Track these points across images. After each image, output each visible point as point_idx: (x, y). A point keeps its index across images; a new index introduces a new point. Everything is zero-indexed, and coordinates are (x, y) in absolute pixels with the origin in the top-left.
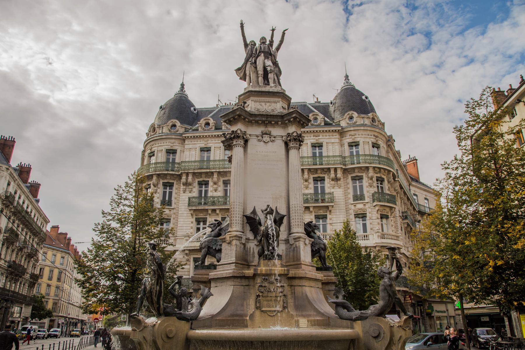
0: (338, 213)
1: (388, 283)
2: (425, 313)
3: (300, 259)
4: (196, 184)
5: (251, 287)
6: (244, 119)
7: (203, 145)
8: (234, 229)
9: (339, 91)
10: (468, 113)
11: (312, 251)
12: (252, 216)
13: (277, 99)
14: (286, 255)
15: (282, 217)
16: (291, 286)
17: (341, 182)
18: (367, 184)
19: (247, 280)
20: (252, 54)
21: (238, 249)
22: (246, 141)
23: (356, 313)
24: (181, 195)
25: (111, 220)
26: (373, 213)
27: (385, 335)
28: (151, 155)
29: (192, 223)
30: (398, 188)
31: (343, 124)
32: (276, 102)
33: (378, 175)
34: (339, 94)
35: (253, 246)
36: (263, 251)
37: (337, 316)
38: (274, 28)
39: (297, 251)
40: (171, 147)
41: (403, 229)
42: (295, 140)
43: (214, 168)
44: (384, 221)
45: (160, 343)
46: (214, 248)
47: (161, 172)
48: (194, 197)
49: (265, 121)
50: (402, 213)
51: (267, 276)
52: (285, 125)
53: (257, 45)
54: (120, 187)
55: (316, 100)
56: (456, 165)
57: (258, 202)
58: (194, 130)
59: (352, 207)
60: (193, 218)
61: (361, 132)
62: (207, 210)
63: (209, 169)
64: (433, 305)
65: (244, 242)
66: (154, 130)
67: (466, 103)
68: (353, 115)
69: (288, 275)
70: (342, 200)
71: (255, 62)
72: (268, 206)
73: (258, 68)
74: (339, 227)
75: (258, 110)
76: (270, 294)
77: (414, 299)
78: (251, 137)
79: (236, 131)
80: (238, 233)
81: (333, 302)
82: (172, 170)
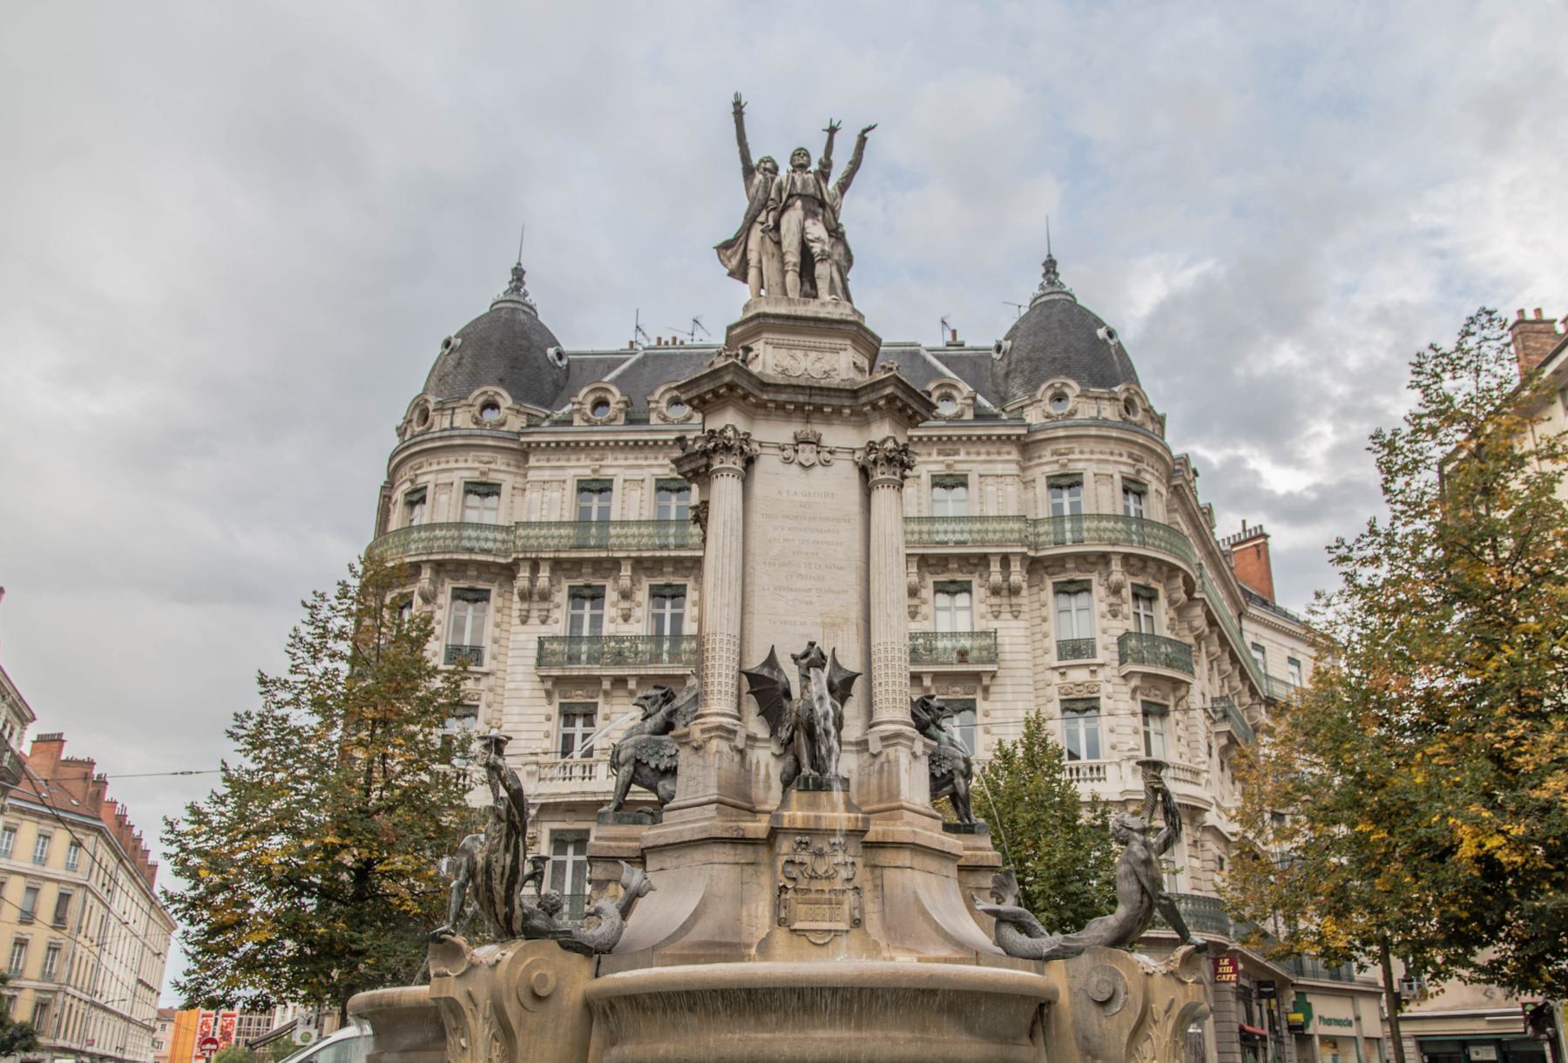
0: (1009, 697)
1: (1142, 855)
2: (1284, 1025)
3: (899, 794)
4: (561, 597)
5: (762, 868)
6: (745, 397)
7: (587, 473)
8: (714, 709)
9: (1024, 311)
10: (1418, 391)
11: (932, 776)
12: (765, 672)
13: (839, 341)
14: (860, 785)
15: (849, 680)
16: (874, 867)
17: (1024, 598)
18: (1104, 608)
19: (750, 849)
20: (767, 199)
21: (725, 765)
22: (750, 461)
23: (1049, 941)
24: (513, 629)
25: (288, 703)
26: (1117, 696)
27: (1130, 997)
28: (416, 497)
29: (549, 719)
30: (1200, 622)
32: (835, 351)
33: (1140, 581)
34: (1023, 319)
35: (767, 761)
36: (798, 769)
37: (1000, 950)
38: (835, 123)
39: (890, 773)
40: (483, 474)
41: (1215, 752)
42: (889, 460)
43: (621, 548)
44: (1154, 725)
45: (512, 1009)
46: (653, 765)
47: (447, 556)
48: (555, 638)
49: (805, 404)
50: (1213, 700)
51: (809, 834)
52: (861, 419)
53: (783, 174)
54: (322, 596)
55: (949, 338)
56: (1369, 552)
57: (781, 633)
58: (556, 423)
59: (1055, 677)
60: (550, 703)
62: (597, 680)
63: (606, 548)
64: (1309, 999)
65: (741, 745)
66: (425, 417)
67: (1415, 360)
68: (1067, 391)
69: (865, 832)
70: (1024, 656)
71: (777, 227)
72: (812, 644)
73: (785, 243)
74: (1013, 735)
75: (784, 371)
76: (816, 885)
77: (1245, 974)
78: (765, 451)
79: (722, 431)
80: (725, 721)
81: (988, 912)
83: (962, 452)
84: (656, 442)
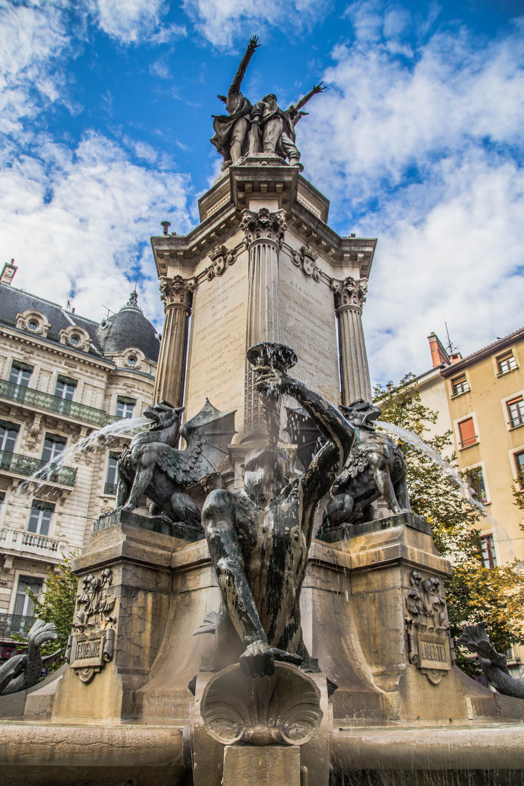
0: (75, 507)
31: (119, 362)
59: (101, 502)
61: (143, 386)
82: (65, 413)
83: (78, 368)
84: (25, 341)
